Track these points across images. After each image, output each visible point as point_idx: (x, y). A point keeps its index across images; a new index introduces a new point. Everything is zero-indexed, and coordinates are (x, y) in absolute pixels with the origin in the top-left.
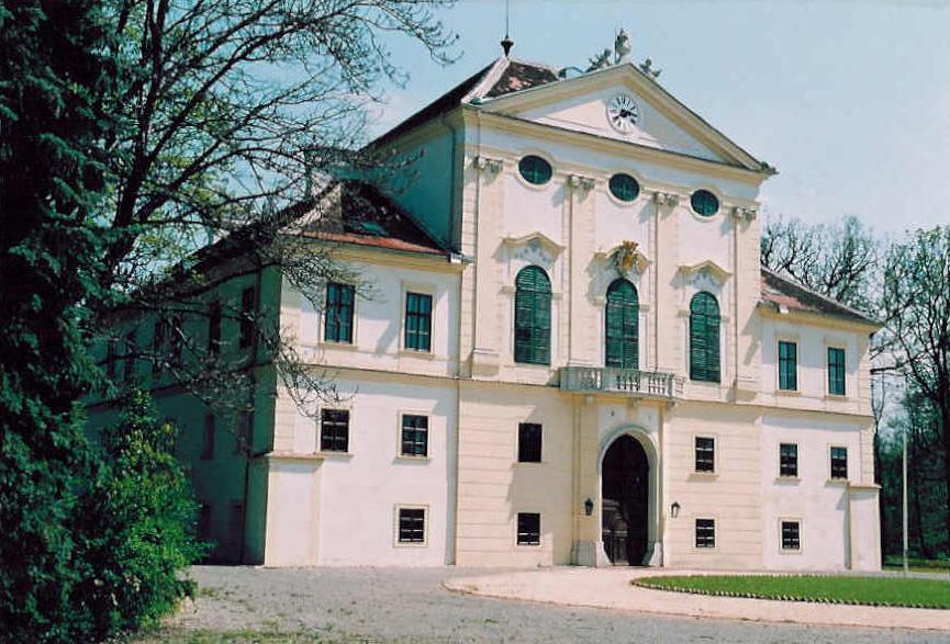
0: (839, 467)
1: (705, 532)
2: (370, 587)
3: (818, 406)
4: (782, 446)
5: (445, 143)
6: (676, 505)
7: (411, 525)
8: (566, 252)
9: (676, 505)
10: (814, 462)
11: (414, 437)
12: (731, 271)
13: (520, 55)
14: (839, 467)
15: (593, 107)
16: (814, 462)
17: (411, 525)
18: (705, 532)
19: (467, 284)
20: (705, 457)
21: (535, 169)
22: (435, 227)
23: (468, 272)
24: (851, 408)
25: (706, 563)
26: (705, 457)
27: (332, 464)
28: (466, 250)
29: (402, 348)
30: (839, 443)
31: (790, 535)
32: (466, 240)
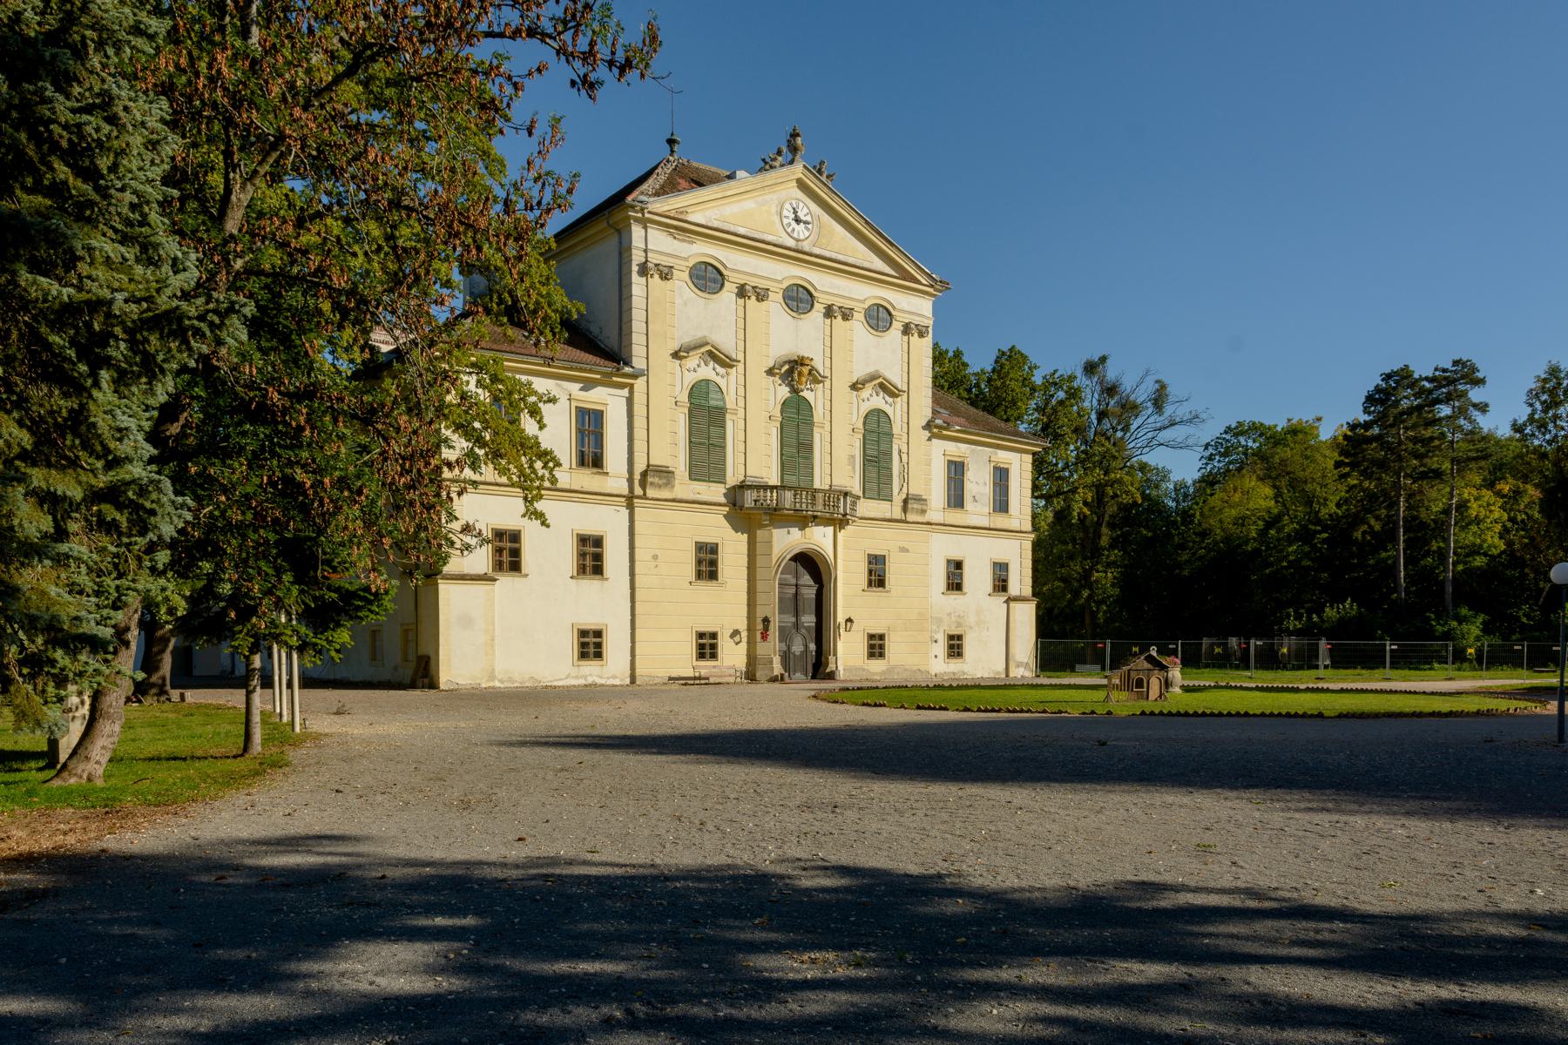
0: (1001, 585)
1: (876, 646)
2: (680, 848)
3: (984, 522)
4: (995, 564)
5: (612, 243)
6: (849, 620)
7: (590, 645)
8: (741, 366)
9: (849, 620)
10: (978, 578)
11: (590, 555)
12: (905, 388)
13: (681, 155)
14: (1001, 585)
15: (559, 386)
16: (978, 578)
17: (590, 645)
18: (876, 646)
19: (639, 398)
20: (877, 577)
21: (708, 278)
22: (610, 339)
23: (639, 384)
24: (1014, 525)
25: (876, 669)
26: (877, 577)
27: (506, 581)
28: (638, 362)
29: (574, 466)
30: (591, 529)
31: (955, 647)
32: (638, 351)
